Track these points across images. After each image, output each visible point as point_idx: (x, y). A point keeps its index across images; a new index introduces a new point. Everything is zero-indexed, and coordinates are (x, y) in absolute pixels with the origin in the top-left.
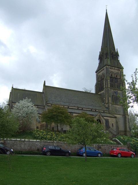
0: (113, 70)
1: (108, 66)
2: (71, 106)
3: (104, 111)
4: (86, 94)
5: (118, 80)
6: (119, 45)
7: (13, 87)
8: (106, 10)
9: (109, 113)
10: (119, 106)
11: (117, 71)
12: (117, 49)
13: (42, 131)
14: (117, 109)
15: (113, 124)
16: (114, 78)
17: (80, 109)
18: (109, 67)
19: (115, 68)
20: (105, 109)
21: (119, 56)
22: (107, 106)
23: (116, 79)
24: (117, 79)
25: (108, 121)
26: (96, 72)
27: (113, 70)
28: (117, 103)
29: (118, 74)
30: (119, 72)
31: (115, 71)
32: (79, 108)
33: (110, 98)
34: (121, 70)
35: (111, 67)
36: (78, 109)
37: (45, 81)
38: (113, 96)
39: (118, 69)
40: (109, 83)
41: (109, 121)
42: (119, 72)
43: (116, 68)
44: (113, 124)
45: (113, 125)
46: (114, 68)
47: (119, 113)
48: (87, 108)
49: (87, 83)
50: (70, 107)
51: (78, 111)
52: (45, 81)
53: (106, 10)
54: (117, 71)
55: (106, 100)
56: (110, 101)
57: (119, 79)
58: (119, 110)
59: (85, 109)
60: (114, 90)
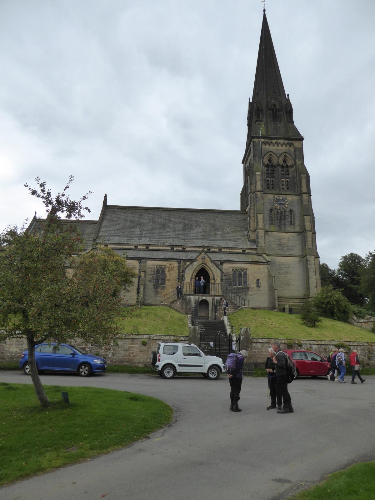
0: (271, 148)
1: (259, 138)
2: (153, 245)
3: (244, 251)
4: (107, 204)
5: (290, 170)
6: (295, 84)
7: (35, 217)
8: (264, 11)
9: (257, 254)
10: (289, 234)
11: (284, 148)
12: (288, 95)
13: (66, 313)
14: (284, 241)
15: (258, 280)
16: (278, 165)
17: (177, 251)
18: (263, 140)
19: (279, 141)
20: (249, 245)
21: (250, 102)
22: (253, 236)
23: (285, 167)
24: (287, 167)
25: (245, 274)
26: (243, 163)
27: (271, 148)
28: (283, 227)
29: (288, 155)
30: (292, 149)
31: (278, 148)
32: (175, 249)
33: (260, 217)
34: (297, 144)
35: (267, 140)
36: (172, 250)
37: (106, 196)
38: (271, 210)
39: (286, 142)
40: (258, 178)
41: (249, 272)
42: (292, 149)
43: (282, 142)
44: (258, 280)
45: (261, 281)
46: (274, 141)
47: (289, 253)
48: (195, 247)
49: (224, 189)
50: (151, 248)
51: (136, 252)
52: (106, 196)
53: (264, 11)
54: (284, 148)
55: (251, 221)
56: (261, 225)
57: (292, 166)
58: (290, 244)
59: (190, 249)
60: (276, 196)
